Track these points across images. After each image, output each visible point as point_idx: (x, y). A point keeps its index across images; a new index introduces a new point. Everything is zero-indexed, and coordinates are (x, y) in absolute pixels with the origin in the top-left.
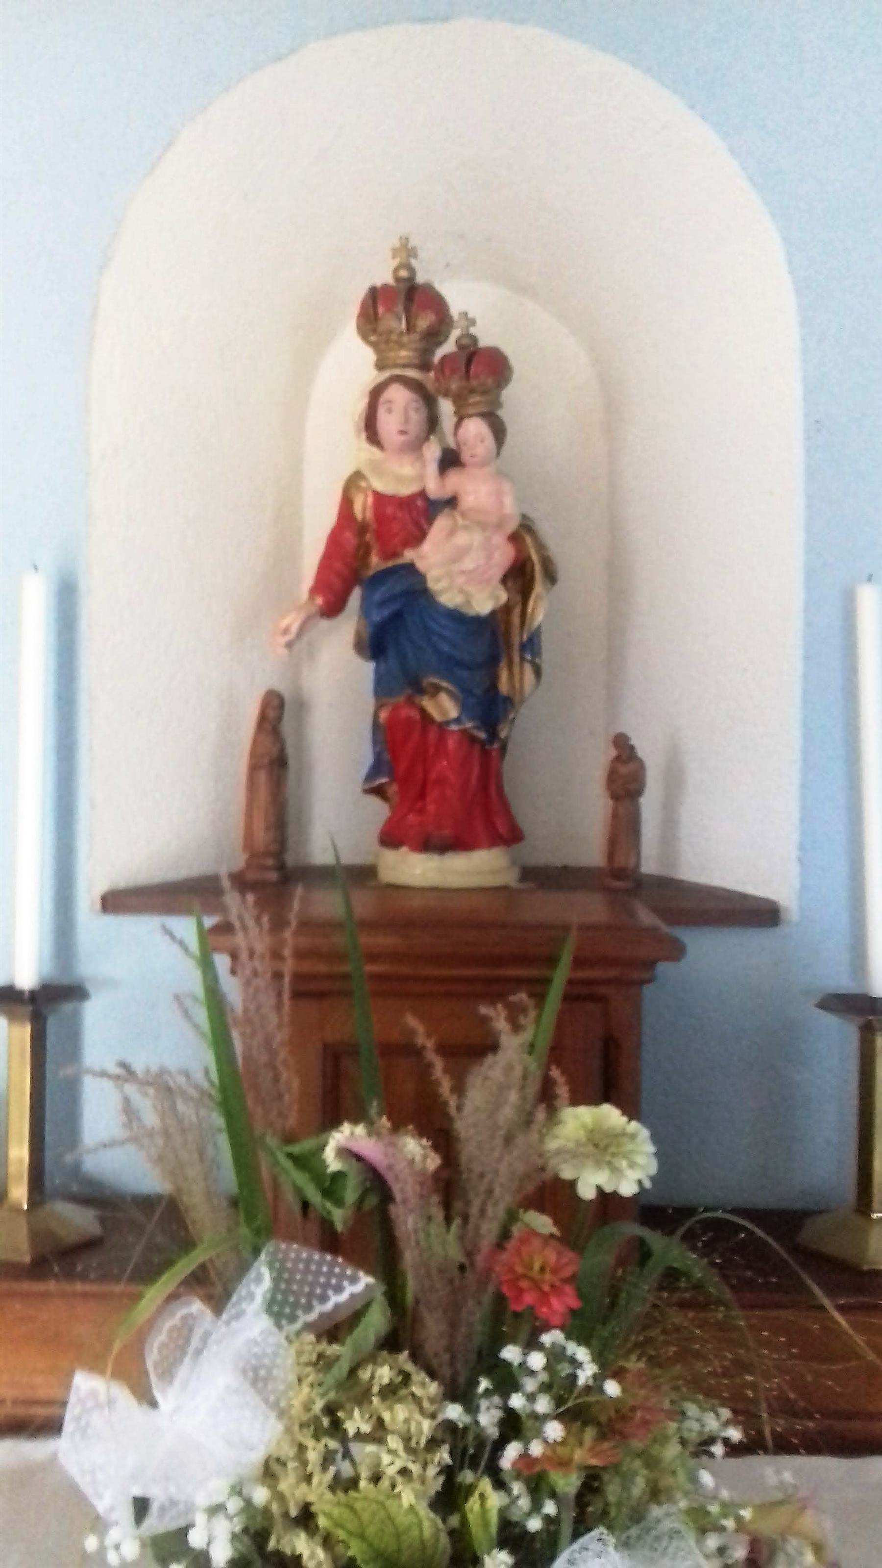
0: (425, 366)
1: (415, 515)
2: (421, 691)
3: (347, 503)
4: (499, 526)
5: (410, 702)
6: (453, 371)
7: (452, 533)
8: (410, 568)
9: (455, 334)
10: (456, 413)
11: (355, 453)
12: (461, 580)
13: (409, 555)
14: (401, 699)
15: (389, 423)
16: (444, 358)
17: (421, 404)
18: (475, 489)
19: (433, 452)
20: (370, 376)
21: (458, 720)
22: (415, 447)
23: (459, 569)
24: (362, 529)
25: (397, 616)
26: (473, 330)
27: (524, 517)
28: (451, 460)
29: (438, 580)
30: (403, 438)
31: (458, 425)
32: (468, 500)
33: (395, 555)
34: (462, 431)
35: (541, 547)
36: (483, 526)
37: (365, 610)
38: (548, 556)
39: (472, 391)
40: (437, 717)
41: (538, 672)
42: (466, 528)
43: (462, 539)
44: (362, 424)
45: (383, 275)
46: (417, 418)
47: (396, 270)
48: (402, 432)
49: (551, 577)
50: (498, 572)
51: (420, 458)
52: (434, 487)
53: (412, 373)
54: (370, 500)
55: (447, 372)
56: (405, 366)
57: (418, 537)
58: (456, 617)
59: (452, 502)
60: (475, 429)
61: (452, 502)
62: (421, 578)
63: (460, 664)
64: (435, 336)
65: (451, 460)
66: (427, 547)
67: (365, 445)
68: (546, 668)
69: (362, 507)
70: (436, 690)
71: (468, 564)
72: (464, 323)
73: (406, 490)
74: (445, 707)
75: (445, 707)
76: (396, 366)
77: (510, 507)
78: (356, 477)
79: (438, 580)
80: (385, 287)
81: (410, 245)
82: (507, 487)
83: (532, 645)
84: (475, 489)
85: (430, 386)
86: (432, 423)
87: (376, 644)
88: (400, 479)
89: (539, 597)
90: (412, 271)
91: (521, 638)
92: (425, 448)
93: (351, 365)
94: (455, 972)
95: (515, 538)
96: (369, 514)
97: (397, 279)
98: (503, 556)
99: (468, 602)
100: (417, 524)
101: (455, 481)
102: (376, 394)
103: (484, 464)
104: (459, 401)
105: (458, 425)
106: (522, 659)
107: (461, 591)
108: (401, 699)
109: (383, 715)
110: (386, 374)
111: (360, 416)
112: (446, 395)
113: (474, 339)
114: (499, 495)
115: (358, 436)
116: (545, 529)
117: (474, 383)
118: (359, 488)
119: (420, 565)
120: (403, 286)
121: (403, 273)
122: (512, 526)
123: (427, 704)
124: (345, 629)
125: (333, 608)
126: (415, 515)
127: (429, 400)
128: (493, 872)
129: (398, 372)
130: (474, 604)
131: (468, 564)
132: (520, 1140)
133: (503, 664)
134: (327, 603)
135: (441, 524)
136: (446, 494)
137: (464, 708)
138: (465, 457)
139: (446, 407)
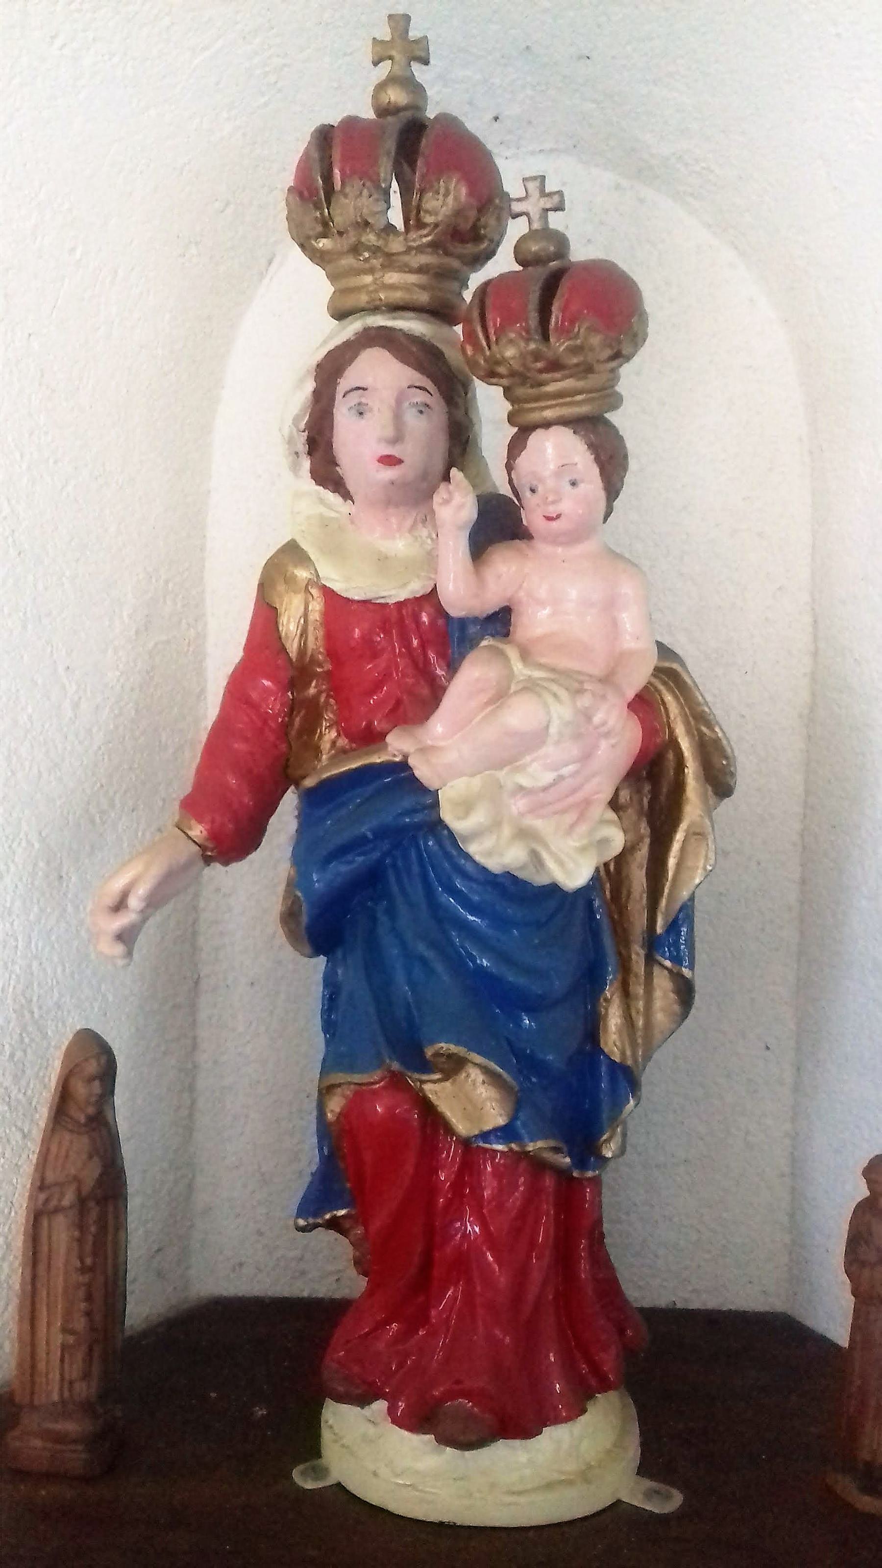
0: (442, 312)
1: (411, 650)
2: (425, 1066)
3: (266, 616)
4: (607, 680)
5: (396, 1082)
6: (510, 318)
7: (500, 697)
8: (400, 774)
9: (516, 229)
10: (512, 419)
11: (292, 504)
12: (519, 805)
13: (398, 744)
14: (374, 1077)
15: (358, 440)
16: (483, 291)
17: (436, 401)
18: (551, 591)
19: (457, 506)
20: (325, 333)
21: (506, 1133)
22: (416, 496)
23: (513, 781)
24: (299, 673)
25: (371, 880)
26: (556, 221)
27: (664, 650)
28: (499, 524)
29: (467, 806)
30: (389, 474)
31: (516, 446)
32: (535, 622)
33: (372, 738)
34: (523, 461)
35: (698, 717)
36: (573, 683)
37: (306, 852)
38: (717, 741)
39: (555, 366)
40: (462, 1127)
41: (685, 992)
42: (530, 687)
43: (521, 715)
44: (301, 444)
45: (351, 94)
46: (424, 430)
47: (381, 87)
48: (389, 461)
49: (720, 783)
50: (603, 786)
51: (429, 518)
52: (461, 590)
53: (413, 325)
54: (317, 607)
55: (494, 320)
56: (396, 308)
57: (422, 699)
58: (508, 887)
59: (500, 622)
60: (557, 451)
61: (500, 622)
62: (428, 799)
63: (517, 1002)
64: (468, 238)
65: (499, 524)
66: (438, 726)
67: (308, 485)
68: (700, 976)
69: (298, 617)
70: (453, 1067)
71: (536, 773)
72: (533, 206)
73: (395, 591)
74: (473, 1101)
75: (473, 1101)
76: (375, 309)
77: (635, 637)
78: (291, 551)
79: (467, 806)
80: (351, 124)
81: (414, 34)
82: (628, 589)
83: (672, 940)
84: (551, 591)
85: (453, 356)
86: (459, 443)
87: (326, 923)
88: (383, 561)
89: (697, 834)
90: (416, 89)
91: (652, 921)
92: (437, 499)
93: (294, 309)
94: (554, 402)
95: (644, 704)
96: (315, 642)
97: (383, 111)
98: (618, 741)
99: (536, 858)
100: (424, 671)
101: (509, 574)
102: (330, 370)
103: (575, 536)
104: (519, 385)
105: (516, 446)
106: (650, 960)
107: (523, 834)
108: (374, 1077)
109: (335, 1105)
110: (353, 327)
111: (296, 420)
112: (490, 376)
113: (561, 242)
114: (610, 606)
115: (295, 468)
116: (697, 669)
117: (559, 346)
118: (290, 581)
119: (422, 771)
120: (393, 124)
121: (396, 96)
122: (638, 676)
123: (437, 1091)
124: (260, 884)
125: (234, 840)
126: (411, 650)
127: (449, 386)
128: (585, 1475)
129: (379, 321)
130: (551, 864)
131: (536, 773)
132: (538, 150)
133: (609, 991)
134: (215, 836)
135: (473, 676)
136: (490, 600)
137: (519, 1103)
138: (532, 516)
139: (490, 403)
